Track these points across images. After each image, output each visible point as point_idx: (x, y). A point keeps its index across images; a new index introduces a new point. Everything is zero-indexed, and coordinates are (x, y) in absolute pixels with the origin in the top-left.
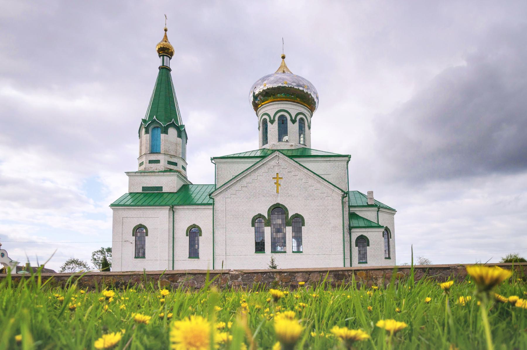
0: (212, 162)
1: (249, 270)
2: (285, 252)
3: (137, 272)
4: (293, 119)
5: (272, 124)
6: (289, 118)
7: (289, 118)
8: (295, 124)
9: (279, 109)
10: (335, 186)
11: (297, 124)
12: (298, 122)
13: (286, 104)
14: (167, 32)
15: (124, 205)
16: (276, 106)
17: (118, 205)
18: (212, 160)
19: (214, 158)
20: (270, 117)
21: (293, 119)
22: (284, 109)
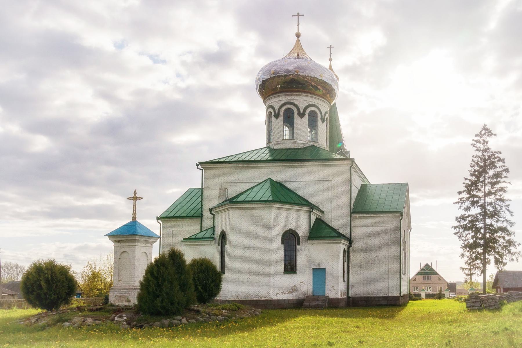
0: (198, 168)
1: (342, 316)
2: (424, 280)
3: (227, 304)
4: (302, 111)
5: (277, 119)
6: (296, 112)
7: (296, 112)
8: (304, 118)
9: (285, 101)
10: (187, 209)
11: (306, 119)
12: (308, 116)
13: (283, 95)
14: (331, 62)
15: (179, 217)
16: (278, 99)
17: (166, 217)
18: (197, 165)
19: (201, 163)
20: (322, 114)
21: (302, 111)
22: (291, 101)
